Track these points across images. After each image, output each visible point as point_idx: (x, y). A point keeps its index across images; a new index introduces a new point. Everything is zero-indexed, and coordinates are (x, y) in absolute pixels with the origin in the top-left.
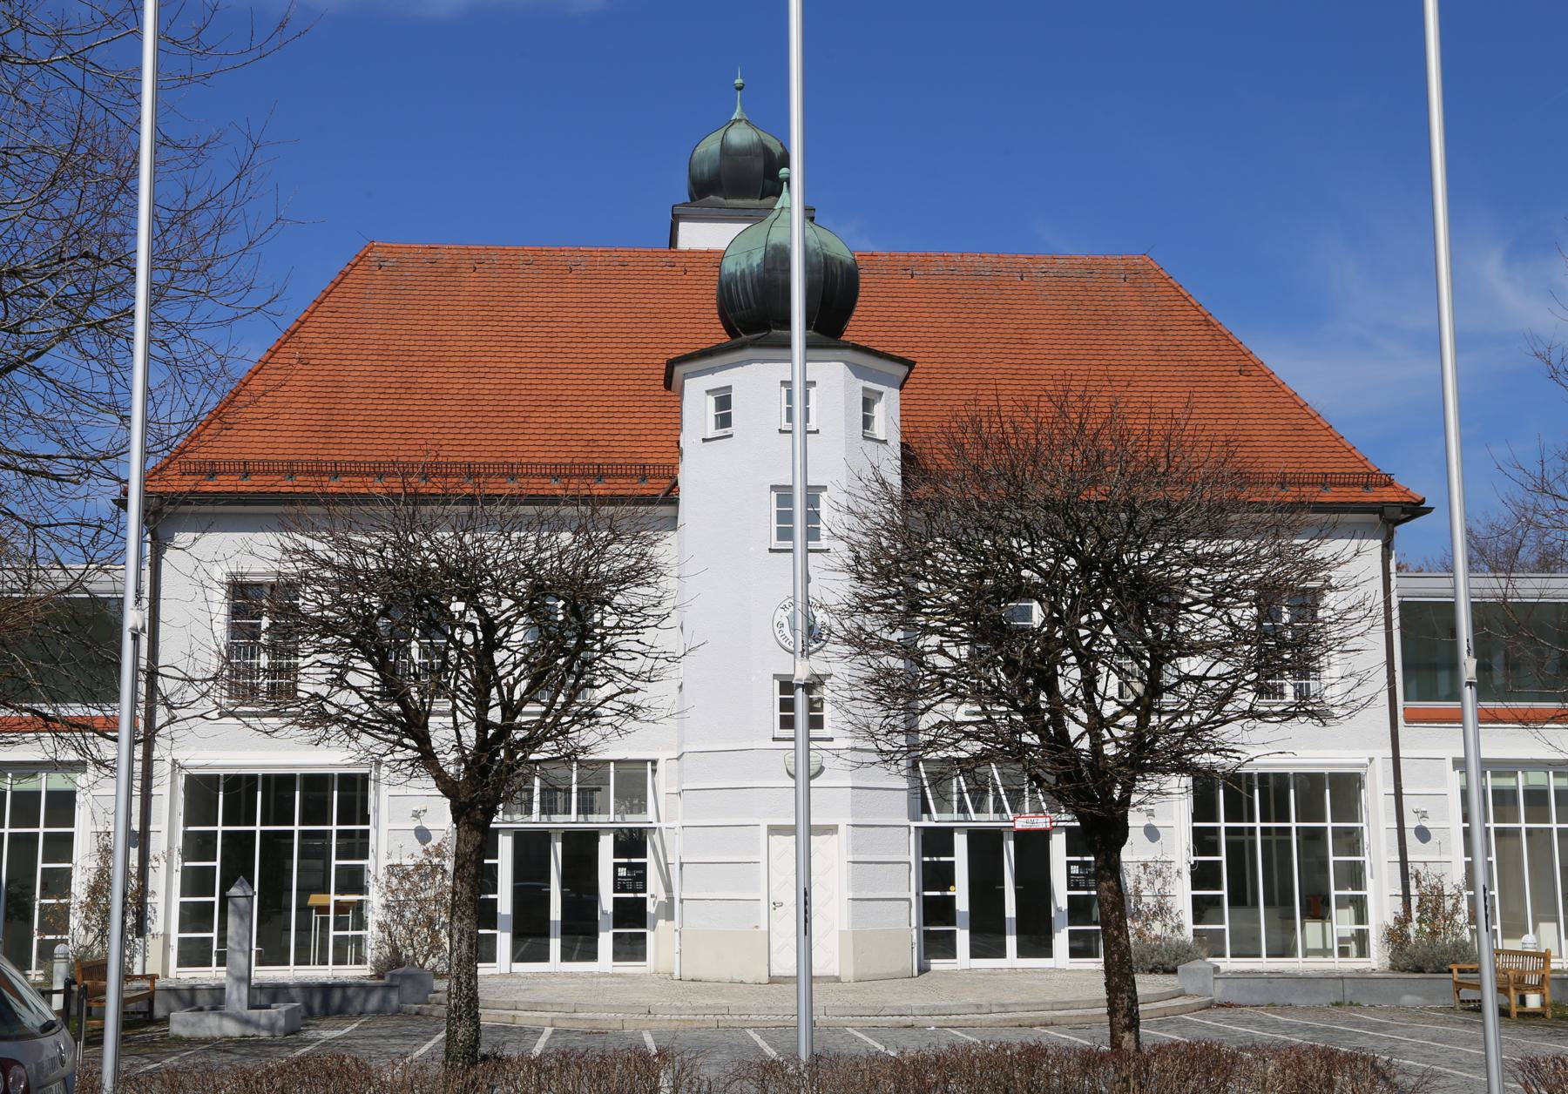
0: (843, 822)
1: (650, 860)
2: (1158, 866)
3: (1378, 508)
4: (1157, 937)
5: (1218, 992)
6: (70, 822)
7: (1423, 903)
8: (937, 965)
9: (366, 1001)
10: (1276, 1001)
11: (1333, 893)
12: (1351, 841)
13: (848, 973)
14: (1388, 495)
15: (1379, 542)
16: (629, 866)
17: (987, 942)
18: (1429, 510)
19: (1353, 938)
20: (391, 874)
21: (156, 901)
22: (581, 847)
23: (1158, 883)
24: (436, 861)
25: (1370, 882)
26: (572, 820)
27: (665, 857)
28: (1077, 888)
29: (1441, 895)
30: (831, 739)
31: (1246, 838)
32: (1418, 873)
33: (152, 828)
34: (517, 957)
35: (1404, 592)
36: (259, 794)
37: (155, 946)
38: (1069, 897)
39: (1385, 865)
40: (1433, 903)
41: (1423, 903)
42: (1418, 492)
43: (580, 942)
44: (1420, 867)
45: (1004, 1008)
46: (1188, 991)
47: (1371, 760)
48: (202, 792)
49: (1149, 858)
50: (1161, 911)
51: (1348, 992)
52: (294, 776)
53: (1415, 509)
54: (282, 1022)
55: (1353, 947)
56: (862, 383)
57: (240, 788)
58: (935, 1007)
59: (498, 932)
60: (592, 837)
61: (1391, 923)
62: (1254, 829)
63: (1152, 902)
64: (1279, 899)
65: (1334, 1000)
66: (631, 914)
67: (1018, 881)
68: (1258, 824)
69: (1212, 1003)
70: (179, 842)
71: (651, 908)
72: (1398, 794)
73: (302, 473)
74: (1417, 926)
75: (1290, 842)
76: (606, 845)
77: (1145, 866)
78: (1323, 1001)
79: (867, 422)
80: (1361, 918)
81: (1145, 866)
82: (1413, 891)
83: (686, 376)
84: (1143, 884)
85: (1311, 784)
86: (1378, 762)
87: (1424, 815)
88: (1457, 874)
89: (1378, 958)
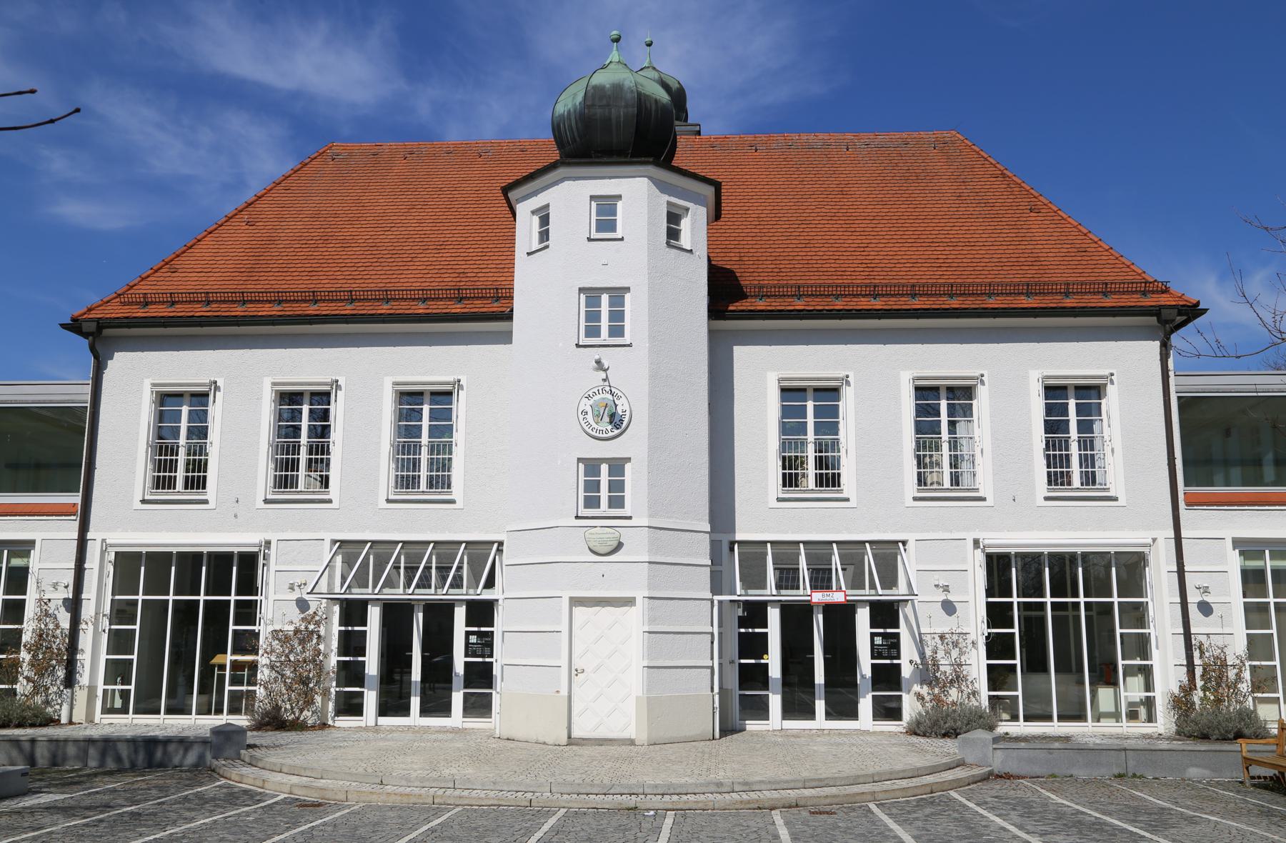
0: (640, 594)
1: (903, 630)
2: (955, 637)
3: (1156, 312)
4: (954, 703)
5: (998, 761)
7: (1207, 671)
8: (752, 725)
10: (1056, 771)
11: (1121, 663)
12: (1137, 615)
13: (641, 736)
14: (1164, 300)
15: (1158, 343)
16: (884, 636)
17: (797, 707)
18: (1205, 311)
19: (1142, 703)
20: (274, 638)
21: (84, 658)
23: (955, 653)
24: (311, 627)
25: (1155, 653)
26: (430, 594)
28: (880, 656)
29: (1224, 665)
30: (630, 518)
31: (1070, 613)
32: (1201, 644)
35: (1180, 388)
37: (81, 696)
38: (873, 665)
39: (1169, 638)
40: (1217, 672)
41: (1207, 671)
42: (1192, 297)
44: (1203, 639)
45: (748, 786)
46: (969, 760)
47: (1154, 540)
48: (127, 564)
49: (946, 630)
51: (1131, 763)
53: (1192, 312)
55: (1143, 711)
56: (666, 198)
57: (158, 561)
58: (670, 785)
61: (1176, 691)
62: (1078, 603)
63: (948, 669)
64: (1068, 665)
65: (1116, 772)
66: (481, 675)
67: (826, 650)
68: (1082, 599)
69: (991, 773)
70: (107, 610)
71: (906, 671)
72: (1181, 572)
74: (1201, 694)
77: (942, 637)
78: (1105, 772)
79: (673, 234)
80: (1149, 686)
81: (942, 637)
82: (1197, 661)
83: (518, 201)
84: (940, 654)
85: (220, 561)
86: (1161, 542)
87: (1206, 590)
88: (1237, 645)
89: (1165, 722)
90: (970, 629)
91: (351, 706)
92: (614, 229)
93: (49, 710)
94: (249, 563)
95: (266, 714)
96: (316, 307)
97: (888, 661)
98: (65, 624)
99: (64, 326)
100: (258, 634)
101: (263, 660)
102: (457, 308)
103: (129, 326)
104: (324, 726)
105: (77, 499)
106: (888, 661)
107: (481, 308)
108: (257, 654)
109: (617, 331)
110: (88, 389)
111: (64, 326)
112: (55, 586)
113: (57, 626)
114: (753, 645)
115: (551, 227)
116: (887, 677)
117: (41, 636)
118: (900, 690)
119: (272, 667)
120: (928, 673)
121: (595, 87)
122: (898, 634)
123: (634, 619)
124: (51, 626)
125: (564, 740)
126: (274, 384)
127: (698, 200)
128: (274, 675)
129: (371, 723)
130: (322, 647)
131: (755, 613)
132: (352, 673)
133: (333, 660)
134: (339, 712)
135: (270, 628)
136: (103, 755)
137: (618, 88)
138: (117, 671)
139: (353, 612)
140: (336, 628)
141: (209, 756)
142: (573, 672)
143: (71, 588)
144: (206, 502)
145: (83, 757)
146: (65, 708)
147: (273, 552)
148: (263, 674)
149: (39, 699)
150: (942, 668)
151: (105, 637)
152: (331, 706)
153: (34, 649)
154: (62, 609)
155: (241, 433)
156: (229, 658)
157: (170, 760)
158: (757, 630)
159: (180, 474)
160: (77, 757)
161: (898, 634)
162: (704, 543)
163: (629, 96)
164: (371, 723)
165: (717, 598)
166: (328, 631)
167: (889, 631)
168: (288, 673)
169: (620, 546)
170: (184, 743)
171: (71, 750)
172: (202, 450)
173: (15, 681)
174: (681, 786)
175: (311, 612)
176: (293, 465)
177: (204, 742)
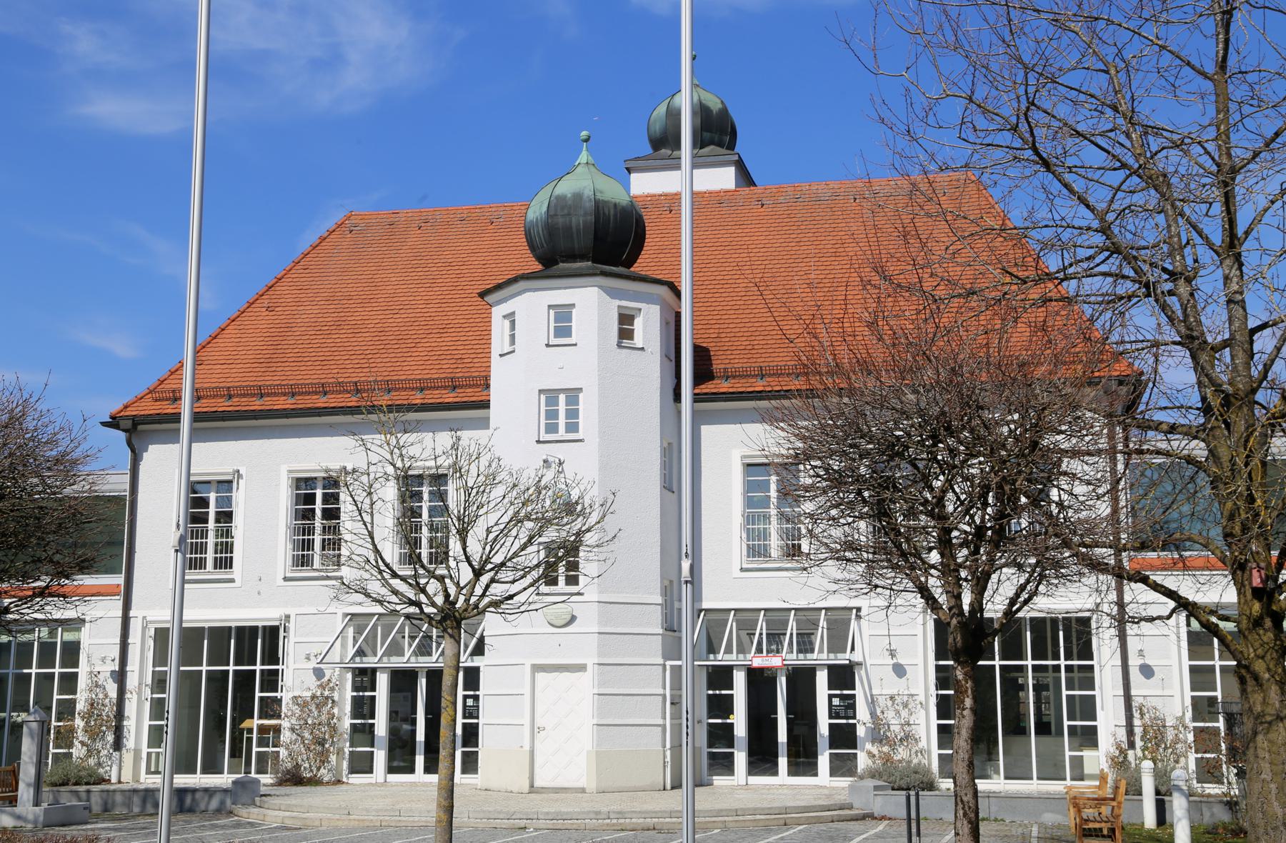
0: (590, 661)
1: (859, 692)
6: (76, 665)
8: (719, 781)
9: (208, 803)
12: (1085, 677)
17: (762, 759)
21: (130, 724)
22: (801, 680)
24: (326, 693)
27: (870, 689)
28: (838, 717)
31: (1051, 674)
33: (128, 668)
34: (391, 770)
36: (1061, 633)
37: (128, 758)
43: (803, 760)
50: (907, 738)
51: (993, 809)
52: (203, 628)
54: (41, 819)
56: (618, 302)
59: (375, 750)
60: (810, 672)
67: (789, 710)
68: (1062, 662)
70: (149, 680)
71: (861, 731)
73: (238, 396)
75: (1060, 678)
76: (822, 678)
77: (892, 698)
79: (625, 334)
81: (892, 698)
82: (1137, 722)
85: (246, 635)
90: (919, 690)
91: (362, 765)
92: (570, 335)
93: (101, 771)
94: (272, 634)
95: (288, 772)
96: (325, 399)
97: (844, 721)
98: (113, 694)
99: (104, 424)
100: (281, 700)
101: (285, 724)
102: (449, 397)
103: (159, 422)
104: (339, 782)
105: (119, 580)
106: (844, 721)
107: (466, 397)
108: (279, 717)
109: (573, 427)
110: (127, 478)
111: (104, 424)
112: (103, 660)
113: (106, 696)
114: (721, 706)
115: (516, 332)
116: (844, 737)
117: (92, 705)
118: (855, 748)
119: (293, 730)
120: (879, 735)
121: (558, 198)
122: (854, 696)
123: (585, 684)
124: (101, 696)
125: (526, 788)
126: (290, 471)
127: (649, 299)
128: (294, 737)
129: (381, 779)
130: (336, 711)
131: (721, 677)
132: (363, 733)
133: (347, 722)
134: (353, 770)
135: (291, 695)
136: (144, 801)
137: (578, 197)
138: (156, 736)
139: (365, 678)
140: (349, 694)
141: (228, 802)
142: (534, 730)
143: (117, 661)
144: (232, 581)
145: (128, 805)
146: (115, 768)
147: (291, 626)
148: (286, 736)
149: (92, 761)
150: (892, 728)
151: (147, 705)
152: (345, 764)
153: (87, 716)
154: (110, 681)
155: (263, 519)
156: (256, 722)
157: (198, 805)
158: (724, 692)
159: (210, 556)
160: (124, 804)
161: (854, 696)
162: (656, 615)
163: (588, 205)
164: (381, 779)
165: (669, 663)
166: (342, 696)
167: (845, 692)
168: (307, 735)
169: (573, 619)
170: (209, 792)
171: (119, 798)
172: (228, 533)
173: (71, 746)
174: (567, 813)
175: (326, 679)
176: (308, 545)
177: (225, 791)
